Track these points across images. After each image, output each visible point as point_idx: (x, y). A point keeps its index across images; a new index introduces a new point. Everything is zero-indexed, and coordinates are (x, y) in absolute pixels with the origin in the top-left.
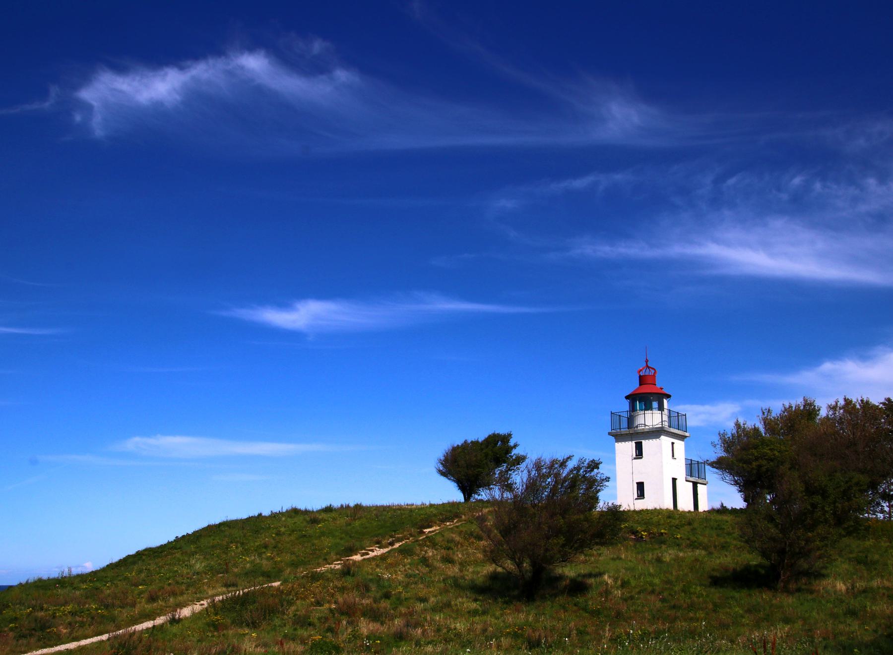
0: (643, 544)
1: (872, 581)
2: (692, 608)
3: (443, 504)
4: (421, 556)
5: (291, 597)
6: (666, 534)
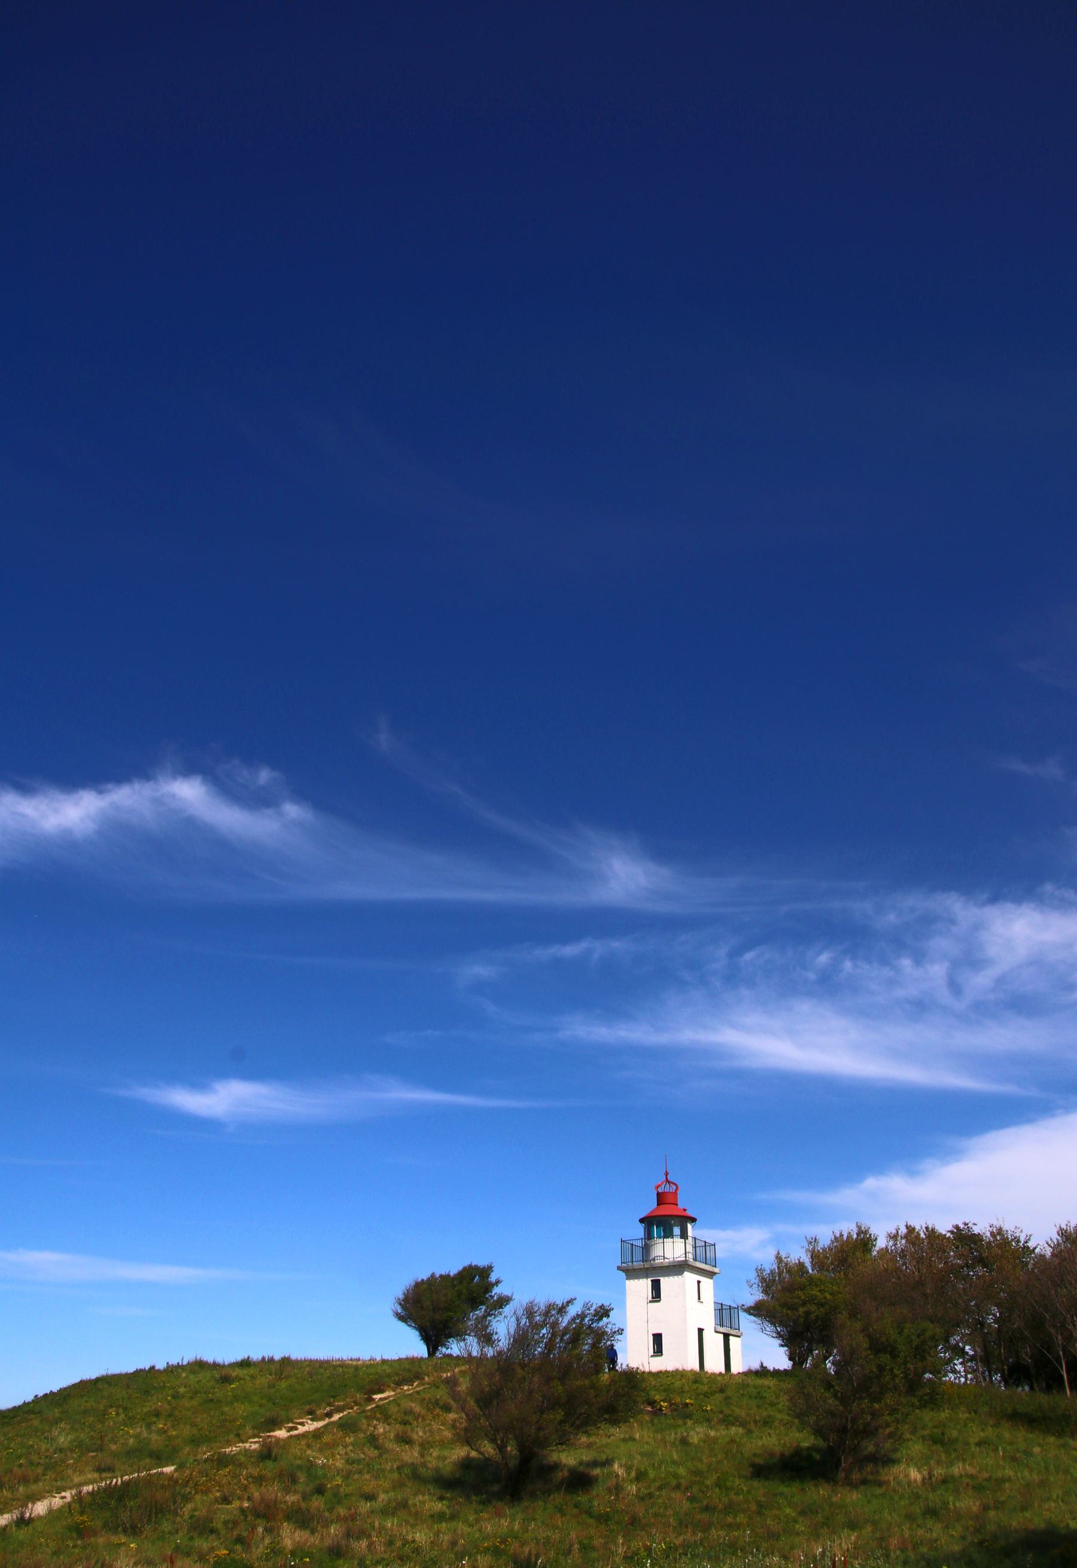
0: (662, 1418)
1: (952, 1467)
2: (730, 1511)
3: (400, 1360)
4: (369, 1433)
5: (188, 1490)
6: (692, 1404)
